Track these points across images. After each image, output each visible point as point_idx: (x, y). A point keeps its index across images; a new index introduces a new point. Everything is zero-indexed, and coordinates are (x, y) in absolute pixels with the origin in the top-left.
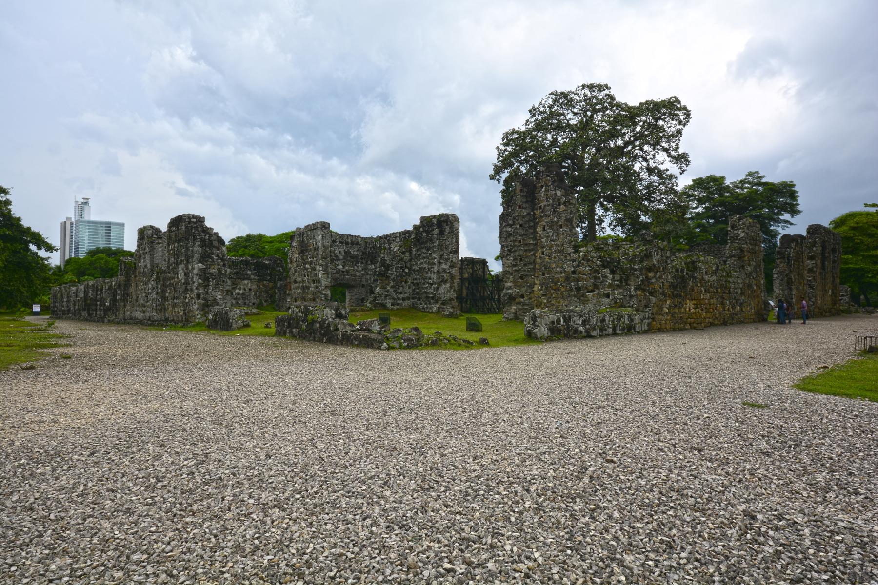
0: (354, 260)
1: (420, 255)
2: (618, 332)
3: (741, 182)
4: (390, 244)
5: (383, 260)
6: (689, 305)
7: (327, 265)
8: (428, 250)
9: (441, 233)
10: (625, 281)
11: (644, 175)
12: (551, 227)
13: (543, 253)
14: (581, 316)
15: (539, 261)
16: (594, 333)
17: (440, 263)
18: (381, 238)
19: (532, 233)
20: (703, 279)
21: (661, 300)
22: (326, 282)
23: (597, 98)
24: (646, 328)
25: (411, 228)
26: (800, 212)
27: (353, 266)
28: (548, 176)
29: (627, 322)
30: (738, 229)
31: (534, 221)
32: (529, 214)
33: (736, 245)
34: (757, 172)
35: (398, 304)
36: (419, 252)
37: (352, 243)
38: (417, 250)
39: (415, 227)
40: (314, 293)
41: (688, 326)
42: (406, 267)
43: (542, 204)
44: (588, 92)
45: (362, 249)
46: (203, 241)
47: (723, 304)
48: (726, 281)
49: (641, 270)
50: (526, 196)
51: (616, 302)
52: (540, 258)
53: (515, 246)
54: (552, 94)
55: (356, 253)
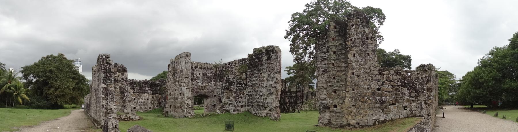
0: (210, 79)
1: (253, 75)
4: (232, 68)
5: (228, 79)
7: (188, 82)
8: (259, 71)
9: (269, 59)
12: (360, 55)
15: (349, 79)
18: (226, 64)
22: (188, 94)
25: (246, 57)
28: (357, 18)
31: (346, 50)
32: (341, 44)
35: (238, 110)
38: (251, 72)
39: (249, 56)
40: (181, 103)
43: (353, 38)
45: (214, 72)
46: (105, 69)
50: (339, 32)
51: (412, 113)
52: (351, 77)
53: (329, 67)
55: (210, 75)
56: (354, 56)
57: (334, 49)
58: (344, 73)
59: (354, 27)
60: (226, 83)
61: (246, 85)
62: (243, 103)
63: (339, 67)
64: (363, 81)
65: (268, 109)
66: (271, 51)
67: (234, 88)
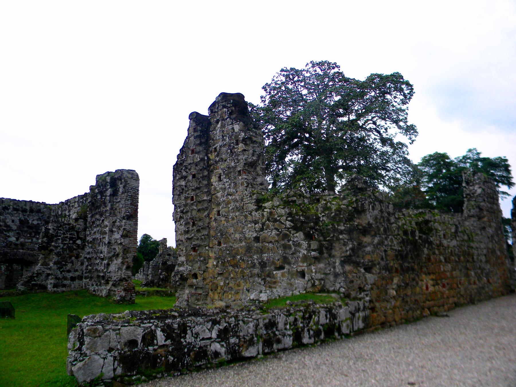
1: (93, 222)
2: (305, 340)
3: (464, 157)
4: (69, 211)
6: (426, 282)
8: (101, 215)
10: (324, 251)
11: (378, 145)
12: (228, 175)
13: (218, 213)
14: (215, 322)
15: (214, 224)
16: (251, 352)
17: (111, 231)
19: (206, 185)
20: (441, 244)
21: (383, 279)
23: (327, 76)
24: (361, 325)
26: (514, 184)
27: (31, 237)
28: (224, 107)
29: (323, 320)
30: (473, 185)
31: (208, 167)
32: (202, 160)
33: (473, 203)
34: (475, 149)
35: (64, 286)
36: (93, 219)
37: (32, 211)
39: (92, 188)
41: (427, 312)
42: (79, 238)
43: (218, 145)
44: (319, 71)
47: (467, 276)
48: (469, 246)
49: (350, 232)
51: (313, 285)
54: (282, 70)
55: (35, 222)
56: (220, 180)
57: (193, 171)
58: (206, 213)
59: (219, 125)
60: (43, 237)
61: (84, 240)
62: (77, 274)
63: (200, 202)
64: (233, 226)
65: (111, 283)
66: (118, 178)
67: (56, 247)
